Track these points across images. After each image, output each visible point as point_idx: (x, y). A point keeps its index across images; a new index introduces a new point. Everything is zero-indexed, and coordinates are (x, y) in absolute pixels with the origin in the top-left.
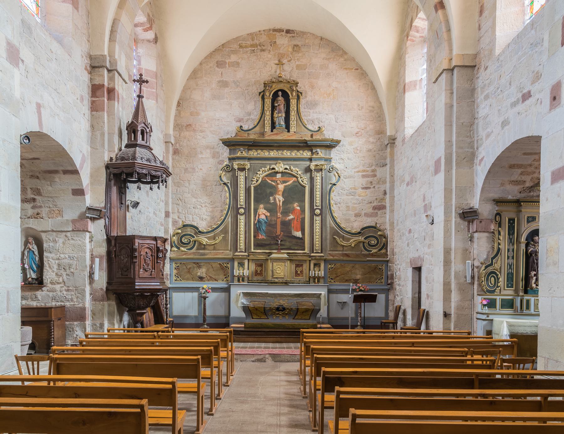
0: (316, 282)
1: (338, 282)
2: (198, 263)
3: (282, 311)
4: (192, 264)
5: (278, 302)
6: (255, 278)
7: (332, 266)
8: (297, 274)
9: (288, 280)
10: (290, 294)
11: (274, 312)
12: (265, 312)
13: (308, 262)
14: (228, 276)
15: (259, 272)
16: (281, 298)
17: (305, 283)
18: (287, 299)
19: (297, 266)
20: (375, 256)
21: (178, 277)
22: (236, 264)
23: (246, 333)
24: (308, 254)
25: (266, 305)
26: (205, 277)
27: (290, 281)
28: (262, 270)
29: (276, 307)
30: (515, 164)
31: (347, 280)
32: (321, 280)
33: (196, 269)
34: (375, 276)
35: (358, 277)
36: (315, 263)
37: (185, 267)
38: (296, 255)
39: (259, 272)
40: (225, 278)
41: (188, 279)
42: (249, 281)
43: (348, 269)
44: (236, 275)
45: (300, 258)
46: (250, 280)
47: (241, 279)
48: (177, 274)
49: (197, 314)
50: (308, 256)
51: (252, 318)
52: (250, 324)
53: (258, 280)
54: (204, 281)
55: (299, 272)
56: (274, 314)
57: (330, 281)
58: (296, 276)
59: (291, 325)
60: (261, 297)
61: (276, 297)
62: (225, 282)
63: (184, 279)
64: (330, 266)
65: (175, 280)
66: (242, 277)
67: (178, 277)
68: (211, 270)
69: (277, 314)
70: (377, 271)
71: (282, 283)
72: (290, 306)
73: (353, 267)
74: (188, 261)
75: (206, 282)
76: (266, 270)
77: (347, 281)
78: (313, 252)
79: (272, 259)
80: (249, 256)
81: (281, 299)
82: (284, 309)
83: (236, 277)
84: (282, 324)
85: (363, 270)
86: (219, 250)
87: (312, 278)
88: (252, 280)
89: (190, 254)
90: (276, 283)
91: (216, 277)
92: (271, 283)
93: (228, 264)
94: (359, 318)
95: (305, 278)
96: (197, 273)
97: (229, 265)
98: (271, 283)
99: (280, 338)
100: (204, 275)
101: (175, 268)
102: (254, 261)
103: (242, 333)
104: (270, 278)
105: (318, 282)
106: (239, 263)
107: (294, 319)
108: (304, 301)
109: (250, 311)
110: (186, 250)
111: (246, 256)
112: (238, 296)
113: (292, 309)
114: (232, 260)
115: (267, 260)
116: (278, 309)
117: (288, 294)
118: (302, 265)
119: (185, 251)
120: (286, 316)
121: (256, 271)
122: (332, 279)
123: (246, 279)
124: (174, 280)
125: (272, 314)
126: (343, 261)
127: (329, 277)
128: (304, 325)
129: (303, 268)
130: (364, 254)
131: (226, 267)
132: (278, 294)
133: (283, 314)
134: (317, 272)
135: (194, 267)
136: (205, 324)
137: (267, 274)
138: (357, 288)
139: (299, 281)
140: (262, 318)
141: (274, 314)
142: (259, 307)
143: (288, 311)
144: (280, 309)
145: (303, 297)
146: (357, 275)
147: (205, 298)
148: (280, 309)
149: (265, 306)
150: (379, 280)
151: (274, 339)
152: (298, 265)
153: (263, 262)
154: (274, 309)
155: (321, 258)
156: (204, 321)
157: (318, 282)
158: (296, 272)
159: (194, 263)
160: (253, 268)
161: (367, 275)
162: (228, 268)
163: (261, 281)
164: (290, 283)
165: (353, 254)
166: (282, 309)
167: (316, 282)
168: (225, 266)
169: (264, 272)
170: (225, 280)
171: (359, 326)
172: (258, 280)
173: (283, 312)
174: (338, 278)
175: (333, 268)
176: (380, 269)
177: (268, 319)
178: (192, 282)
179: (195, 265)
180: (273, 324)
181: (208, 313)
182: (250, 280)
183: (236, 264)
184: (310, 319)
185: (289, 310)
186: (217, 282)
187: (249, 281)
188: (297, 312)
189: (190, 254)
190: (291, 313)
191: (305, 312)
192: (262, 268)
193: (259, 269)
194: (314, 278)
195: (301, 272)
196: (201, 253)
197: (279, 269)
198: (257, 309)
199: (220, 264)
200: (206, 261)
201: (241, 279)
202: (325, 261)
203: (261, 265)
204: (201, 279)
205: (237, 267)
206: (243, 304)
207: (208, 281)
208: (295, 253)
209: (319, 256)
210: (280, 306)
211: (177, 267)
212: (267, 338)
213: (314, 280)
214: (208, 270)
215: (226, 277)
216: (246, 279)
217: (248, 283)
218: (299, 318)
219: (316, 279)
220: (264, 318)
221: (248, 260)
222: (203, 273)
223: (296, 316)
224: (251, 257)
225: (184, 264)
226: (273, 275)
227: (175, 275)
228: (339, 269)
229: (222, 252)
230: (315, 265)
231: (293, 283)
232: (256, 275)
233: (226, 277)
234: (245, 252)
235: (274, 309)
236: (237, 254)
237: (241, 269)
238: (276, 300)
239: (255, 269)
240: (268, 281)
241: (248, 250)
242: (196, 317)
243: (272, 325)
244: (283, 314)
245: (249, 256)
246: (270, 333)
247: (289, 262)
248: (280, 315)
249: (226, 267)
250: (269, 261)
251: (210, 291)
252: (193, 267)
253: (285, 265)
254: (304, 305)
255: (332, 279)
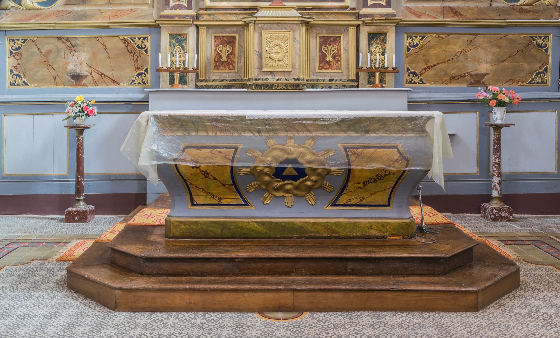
0: (377, 81)
1: (430, 82)
2: (68, 39)
3: (295, 178)
4: (53, 41)
5: (282, 150)
6: (216, 75)
7: (416, 41)
8: (323, 62)
9: (302, 77)
10: (323, 119)
11: (268, 184)
12: (234, 184)
13: (353, 30)
14: (146, 70)
15: (224, 58)
16: (290, 134)
17: (344, 86)
18: (313, 138)
19: (325, 41)
20: (528, 12)
21: (17, 75)
22: (165, 38)
23: (165, 266)
24: (354, 9)
25: (240, 161)
26: (87, 74)
27: (308, 80)
28: (233, 53)
29: (274, 165)
30: (340, 56)
31: (453, 77)
32: (389, 78)
33: (63, 54)
34: (526, 66)
35: (484, 68)
36: (372, 32)
37: (36, 50)
38: (322, 14)
39: (224, 58)
40: (138, 76)
41: (42, 81)
42: (199, 83)
43: (457, 49)
44: (165, 68)
45: (331, 20)
46: (202, 81)
47: (177, 76)
48: (15, 68)
49: (64, 171)
50: (353, 14)
51: (193, 204)
52: (184, 223)
53: (222, 81)
54: (85, 85)
55: (329, 58)
56: (267, 190)
57: (409, 79)
58: (321, 68)
59: (327, 226)
60: (221, 130)
61: (273, 130)
62: (139, 87)
63: (33, 81)
64: (409, 40)
65: (11, 84)
66: (181, 71)
67: (17, 75)
68: (102, 55)
69: (278, 189)
70: (533, 51)
71: (286, 85)
72: (322, 164)
73: (470, 42)
74: (42, 35)
75: (90, 87)
76: (244, 51)
77: (453, 78)
78: (365, 5)
79: (260, 22)
80: (198, 16)
81: (291, 138)
82: (301, 172)
83: (165, 71)
84: (294, 224)
85: (495, 50)
86: (121, 4)
87: (364, 71)
88: (206, 81)
89: (49, 16)
90: (271, 85)
91: (115, 74)
92: (257, 86)
93: (144, 39)
94: (496, 179)
95: (345, 72)
96: (68, 63)
97: (148, 44)
98: (257, 86)
99: (289, 294)
100: (84, 70)
101: (11, 53)
102: (211, 31)
103: (150, 265)
104: (253, 74)
105: (382, 81)
106: (172, 36)
107: (334, 205)
108: (374, 143)
109: (185, 180)
110: (37, 6)
111: (192, 17)
112: (142, 128)
113: (328, 172)
114: (157, 27)
115: (247, 25)
116: (324, 282)
117: (316, 120)
118: (336, 40)
119: (36, 9)
120: (308, 196)
121: (218, 57)
122: (415, 74)
123: (191, 77)
124: (8, 84)
125: (259, 188)
126: (444, 25)
127: (408, 69)
128: (371, 228)
129: (339, 45)
130: (498, 9)
131: (141, 48)
132: (280, 120)
133: (297, 188)
134: (378, 57)
135: (59, 51)
136: (79, 200)
137: (246, 63)
138: (490, 96)
139: (330, 80)
140: (223, 201)
141: (265, 188)
142: (216, 168)
143: (313, 178)
144: (285, 173)
145: (367, 131)
146: (479, 62)
147: (81, 130)
148: (285, 173)
149: (235, 164)
150: (537, 75)
151: (269, 295)
152: (328, 38)
153: (235, 32)
154: (267, 174)
155: (387, 20)
156: (79, 190)
157: (382, 81)
158: (323, 57)
159: (59, 38)
160: (209, 49)
161: (506, 64)
162: (146, 51)
163: (231, 81)
164: (308, 87)
165: (471, 9)
166: (296, 174)
167: (377, 81)
168: (138, 46)
169: (240, 58)
170: (138, 80)
171: (495, 201)
172: (222, 81)
173: (296, 183)
174: (431, 72)
175: (417, 44)
176: (539, 46)
177: (246, 204)
178: (55, 87)
179: (60, 45)
180: (263, 224)
181: (90, 168)
182: (202, 81)
183: (165, 38)
184: (388, 205)
185: (319, 175)
186: (117, 87)
187: (199, 83)
188: (347, 181)
189: (49, 16)
190: (327, 183)
191: (375, 181)
192: (233, 48)
193: (225, 50)
194: (371, 73)
195: (334, 57)
196: (77, 12)
197: (277, 47)
198: (206, 174)
199: (125, 41)
200: (90, 35)
201: (177, 76)
202: (399, 26)
203: (230, 42)
204: (77, 78)
205: (168, 47)
206: (159, 157)
207: (96, 84)
208: (320, 8)
209: (381, 15)
210: (287, 161)
211: (16, 49)
212: (240, 295)
213: (369, 78)
214: (94, 56)
215: (140, 74)
216: (191, 77)
217: (197, 86)
218: (353, 202)
219: (377, 75)
220: (231, 202)
221: (197, 27)
222: (81, 64)
223: (340, 194)
224: (205, 20)
225: (33, 41)
226: (261, 66)
227: (11, 71)
228: (432, 47)
229: (131, 10)
230: (372, 37)
231: (313, 86)
232: (217, 68)
233: (140, 74)
234: (189, 7)
235: (267, 174)
236: (167, 12)
237: (178, 50)
238: (272, 142)
239: (215, 50)
240: (248, 83)
241: (197, 3)
242: (62, 179)
243: (259, 228)
244: (297, 188)
245: (198, 18)
246: (254, 265)
247: (303, 29)
248: (288, 191)
249: (141, 48)
250: (251, 27)
251: (92, 112)
252: (58, 49)
253: (294, 39)
254: (370, 159)
255: (415, 74)
